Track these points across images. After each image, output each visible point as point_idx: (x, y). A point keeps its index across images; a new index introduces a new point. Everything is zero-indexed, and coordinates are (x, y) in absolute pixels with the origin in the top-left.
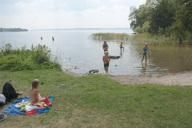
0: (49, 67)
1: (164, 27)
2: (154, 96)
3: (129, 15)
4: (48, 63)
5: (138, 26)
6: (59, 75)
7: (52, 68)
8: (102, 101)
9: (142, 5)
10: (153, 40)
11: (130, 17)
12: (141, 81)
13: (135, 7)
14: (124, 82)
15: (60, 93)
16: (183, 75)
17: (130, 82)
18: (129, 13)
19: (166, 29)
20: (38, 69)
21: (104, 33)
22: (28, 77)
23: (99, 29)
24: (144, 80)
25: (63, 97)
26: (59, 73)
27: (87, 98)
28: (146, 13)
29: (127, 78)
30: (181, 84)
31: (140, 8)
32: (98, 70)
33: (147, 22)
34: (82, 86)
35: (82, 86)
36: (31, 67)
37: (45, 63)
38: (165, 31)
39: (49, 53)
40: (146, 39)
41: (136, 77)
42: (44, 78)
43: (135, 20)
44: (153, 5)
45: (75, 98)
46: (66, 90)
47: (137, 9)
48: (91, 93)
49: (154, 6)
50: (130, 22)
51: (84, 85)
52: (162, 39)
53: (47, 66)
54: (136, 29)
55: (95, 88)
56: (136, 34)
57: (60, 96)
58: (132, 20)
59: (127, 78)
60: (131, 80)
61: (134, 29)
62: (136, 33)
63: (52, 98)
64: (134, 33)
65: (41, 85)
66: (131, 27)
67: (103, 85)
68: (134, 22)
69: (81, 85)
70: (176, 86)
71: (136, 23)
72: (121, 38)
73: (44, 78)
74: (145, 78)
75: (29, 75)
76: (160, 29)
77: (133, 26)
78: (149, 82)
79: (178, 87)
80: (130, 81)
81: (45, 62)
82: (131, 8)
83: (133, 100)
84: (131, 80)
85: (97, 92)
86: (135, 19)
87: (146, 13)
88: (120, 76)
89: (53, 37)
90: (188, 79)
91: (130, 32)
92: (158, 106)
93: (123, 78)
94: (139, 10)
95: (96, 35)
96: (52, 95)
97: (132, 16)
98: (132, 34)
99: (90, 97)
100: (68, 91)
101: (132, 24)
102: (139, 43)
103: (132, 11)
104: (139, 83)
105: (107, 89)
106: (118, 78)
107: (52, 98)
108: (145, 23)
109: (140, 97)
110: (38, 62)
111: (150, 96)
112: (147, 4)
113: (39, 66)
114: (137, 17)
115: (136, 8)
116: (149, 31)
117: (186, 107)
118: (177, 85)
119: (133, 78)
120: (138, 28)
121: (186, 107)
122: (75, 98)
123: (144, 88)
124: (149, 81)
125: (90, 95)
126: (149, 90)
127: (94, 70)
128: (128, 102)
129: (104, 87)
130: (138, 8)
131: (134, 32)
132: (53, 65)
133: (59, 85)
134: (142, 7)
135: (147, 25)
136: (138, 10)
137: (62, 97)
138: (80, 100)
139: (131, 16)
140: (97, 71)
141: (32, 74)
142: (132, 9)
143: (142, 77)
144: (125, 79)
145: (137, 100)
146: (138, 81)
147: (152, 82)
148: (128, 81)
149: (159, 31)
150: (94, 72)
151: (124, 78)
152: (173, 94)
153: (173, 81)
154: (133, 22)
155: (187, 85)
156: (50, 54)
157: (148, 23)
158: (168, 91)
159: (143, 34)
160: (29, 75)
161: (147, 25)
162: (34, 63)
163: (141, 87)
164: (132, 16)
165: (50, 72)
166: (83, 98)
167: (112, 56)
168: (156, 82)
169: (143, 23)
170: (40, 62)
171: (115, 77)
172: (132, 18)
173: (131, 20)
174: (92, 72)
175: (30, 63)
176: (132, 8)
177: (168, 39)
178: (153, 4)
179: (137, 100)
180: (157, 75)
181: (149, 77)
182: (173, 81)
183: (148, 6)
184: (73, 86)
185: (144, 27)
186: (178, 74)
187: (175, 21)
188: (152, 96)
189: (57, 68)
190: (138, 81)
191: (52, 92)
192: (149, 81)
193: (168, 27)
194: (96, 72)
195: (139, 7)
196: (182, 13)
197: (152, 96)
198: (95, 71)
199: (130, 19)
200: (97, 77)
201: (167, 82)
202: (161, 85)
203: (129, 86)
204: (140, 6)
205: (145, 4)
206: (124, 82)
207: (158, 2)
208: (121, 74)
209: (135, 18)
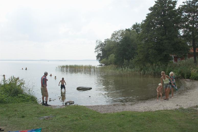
0: (25, 99)
1: (128, 60)
2: (134, 121)
3: (95, 48)
4: (23, 96)
5: (104, 58)
6: (38, 108)
7: (28, 100)
8: (89, 129)
9: (107, 39)
10: (119, 71)
11: (96, 50)
12: (117, 110)
13: (101, 41)
14: (102, 111)
15: (45, 124)
16: (152, 101)
17: (108, 111)
18: (95, 45)
19: (130, 61)
20: (12, 102)
21: (86, 65)
22: (4, 111)
23: (65, 61)
24: (120, 109)
25: (50, 128)
26: (36, 105)
27: (74, 128)
28: (111, 47)
29: (104, 108)
30: (152, 109)
31: (105, 42)
32: (73, 102)
33: (113, 54)
34: (66, 117)
35: (66, 117)
36: (4, 100)
37: (20, 96)
38: (129, 63)
39: (23, 85)
40: (111, 70)
41: (112, 106)
42: (23, 112)
43: (101, 52)
44: (118, 39)
45: (63, 129)
46: (50, 122)
47: (102, 42)
48: (77, 123)
49: (118, 41)
50: (96, 54)
51: (67, 116)
52: (127, 70)
53: (21, 99)
54: (102, 61)
55: (78, 118)
56: (103, 66)
57: (47, 128)
58: (98, 53)
59: (104, 108)
60: (108, 109)
61: (100, 61)
62: (102, 65)
63: (39, 130)
64: (100, 65)
65: (21, 118)
66: (97, 59)
67: (85, 115)
68: (100, 54)
69: (64, 116)
70: (148, 112)
71: (102, 55)
72: (88, 70)
73: (23, 112)
74: (120, 107)
75: (5, 109)
76: (125, 61)
77: (99, 59)
78: (125, 110)
79: (150, 112)
80: (107, 110)
81: (20, 95)
82: (97, 41)
83: (116, 126)
84: (108, 110)
85: (81, 121)
86: (101, 52)
87: (111, 46)
88: (96, 106)
89: (46, 74)
90: (157, 105)
91: (96, 64)
92: (139, 129)
93: (99, 107)
94: (104, 43)
95: (63, 67)
96: (38, 128)
97: (98, 49)
98: (98, 65)
99: (76, 127)
100: (53, 122)
101: (98, 57)
102: (107, 74)
103: (98, 44)
104: (116, 112)
105: (90, 118)
106: (95, 108)
107: (39, 130)
108: (111, 55)
109: (121, 123)
110: (11, 95)
111: (130, 121)
112: (112, 38)
113: (13, 99)
114: (103, 50)
115: (101, 42)
116: (115, 63)
117: (161, 128)
118: (150, 111)
119: (109, 108)
120: (104, 60)
121: (161, 128)
122: (63, 129)
123: (123, 115)
124: (124, 109)
125: (76, 124)
126: (127, 116)
127: (70, 102)
128: (113, 128)
129: (86, 116)
130: (103, 41)
131: (101, 64)
132: (28, 98)
133: (41, 118)
134: (107, 41)
135: (113, 57)
136: (103, 43)
137: (49, 129)
138: (67, 130)
139: (97, 49)
140: (73, 102)
141: (7, 107)
142: (98, 42)
143: (117, 106)
144: (103, 109)
145: (120, 126)
146: (114, 110)
147: (127, 110)
148: (105, 110)
149: (124, 63)
150: (70, 104)
151: (101, 108)
152: (149, 118)
153: (145, 108)
154: (99, 54)
155: (157, 110)
156: (23, 86)
157: (114, 56)
158: (144, 116)
159: (109, 66)
160: (5, 109)
161: (112, 57)
162: (7, 96)
163: (120, 115)
164: (98, 49)
165: (27, 105)
166: (70, 128)
167: (84, 87)
168: (130, 110)
169: (109, 54)
170: (14, 94)
171: (92, 108)
172: (98, 51)
173: (97, 52)
174: (68, 104)
175: (2, 96)
176: (98, 41)
177: (133, 70)
178: (117, 38)
179: (120, 126)
180: (130, 104)
181: (123, 106)
182: (145, 108)
183: (113, 40)
184: (57, 118)
185: (109, 60)
186: (147, 101)
187: (137, 54)
188: (132, 121)
189: (33, 100)
190: (114, 110)
191: (37, 125)
192: (124, 109)
193: (132, 60)
194: (72, 104)
195: (104, 41)
196: (143, 47)
197: (132, 121)
198: (71, 103)
199: (96, 52)
200: (77, 108)
201: (140, 109)
202: (136, 112)
203: (109, 115)
204: (105, 40)
205: (110, 38)
206: (102, 112)
207: (122, 37)
208: (96, 104)
209: (101, 50)
